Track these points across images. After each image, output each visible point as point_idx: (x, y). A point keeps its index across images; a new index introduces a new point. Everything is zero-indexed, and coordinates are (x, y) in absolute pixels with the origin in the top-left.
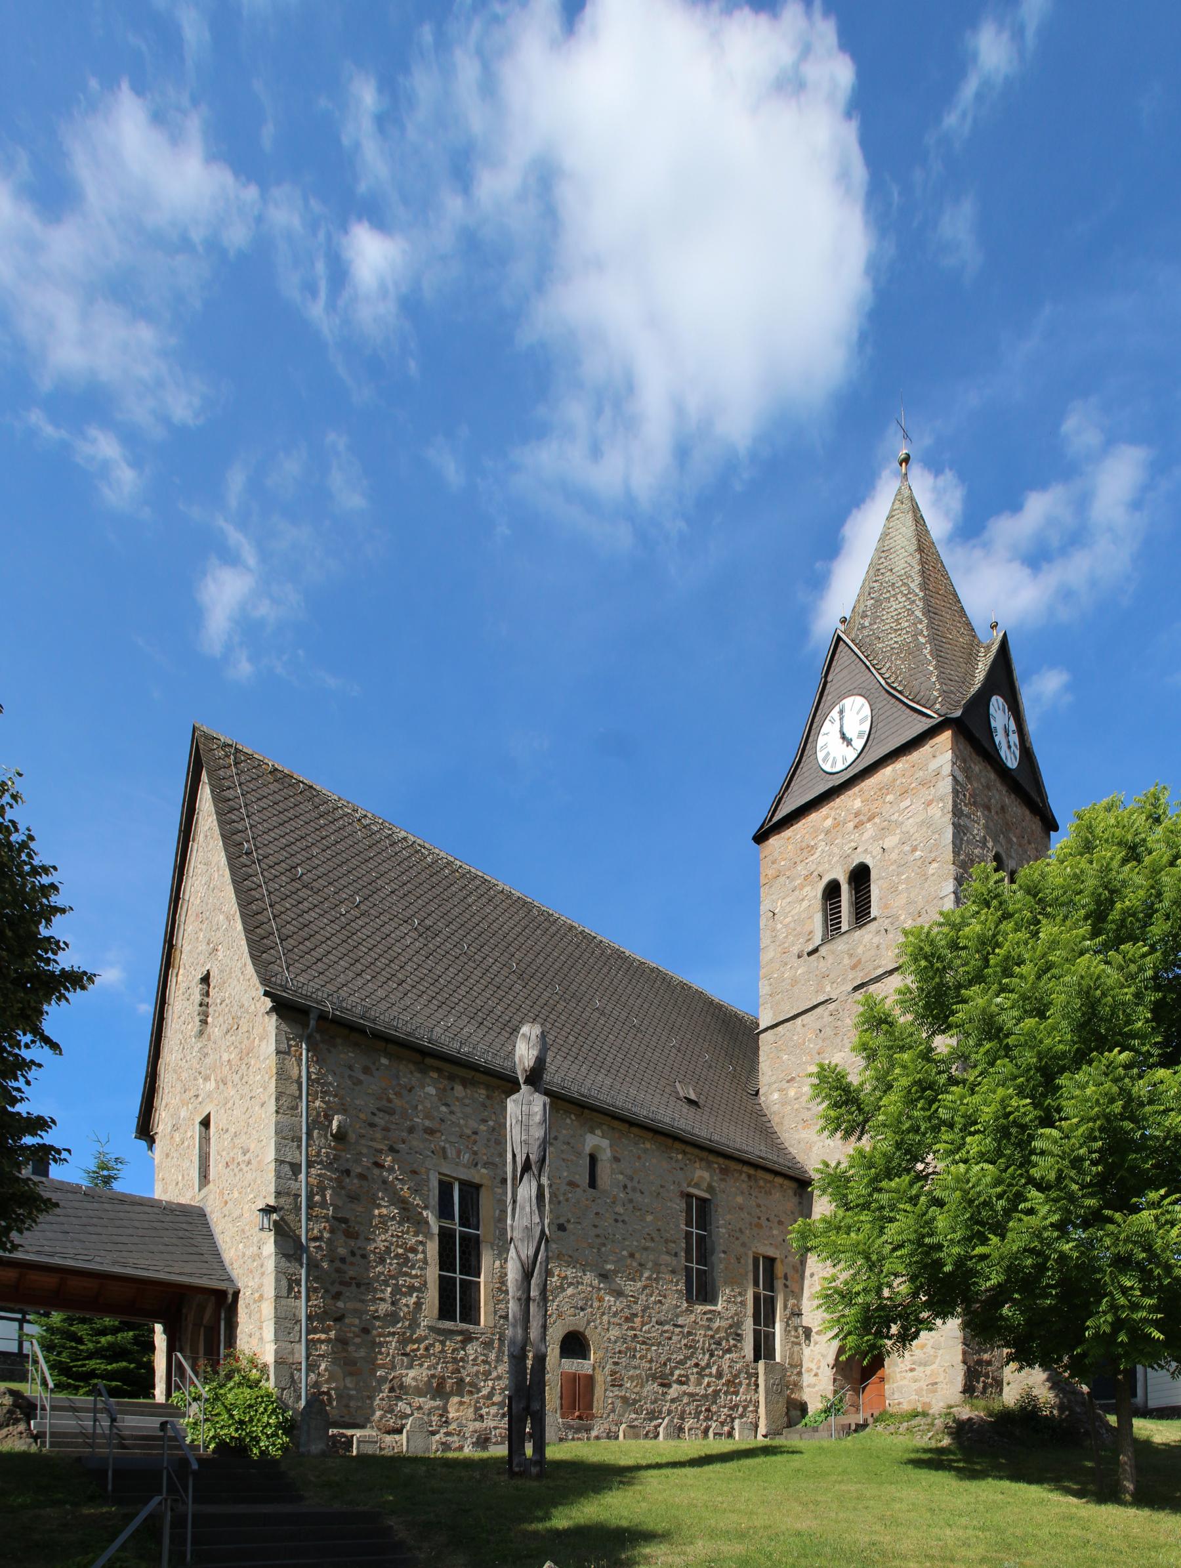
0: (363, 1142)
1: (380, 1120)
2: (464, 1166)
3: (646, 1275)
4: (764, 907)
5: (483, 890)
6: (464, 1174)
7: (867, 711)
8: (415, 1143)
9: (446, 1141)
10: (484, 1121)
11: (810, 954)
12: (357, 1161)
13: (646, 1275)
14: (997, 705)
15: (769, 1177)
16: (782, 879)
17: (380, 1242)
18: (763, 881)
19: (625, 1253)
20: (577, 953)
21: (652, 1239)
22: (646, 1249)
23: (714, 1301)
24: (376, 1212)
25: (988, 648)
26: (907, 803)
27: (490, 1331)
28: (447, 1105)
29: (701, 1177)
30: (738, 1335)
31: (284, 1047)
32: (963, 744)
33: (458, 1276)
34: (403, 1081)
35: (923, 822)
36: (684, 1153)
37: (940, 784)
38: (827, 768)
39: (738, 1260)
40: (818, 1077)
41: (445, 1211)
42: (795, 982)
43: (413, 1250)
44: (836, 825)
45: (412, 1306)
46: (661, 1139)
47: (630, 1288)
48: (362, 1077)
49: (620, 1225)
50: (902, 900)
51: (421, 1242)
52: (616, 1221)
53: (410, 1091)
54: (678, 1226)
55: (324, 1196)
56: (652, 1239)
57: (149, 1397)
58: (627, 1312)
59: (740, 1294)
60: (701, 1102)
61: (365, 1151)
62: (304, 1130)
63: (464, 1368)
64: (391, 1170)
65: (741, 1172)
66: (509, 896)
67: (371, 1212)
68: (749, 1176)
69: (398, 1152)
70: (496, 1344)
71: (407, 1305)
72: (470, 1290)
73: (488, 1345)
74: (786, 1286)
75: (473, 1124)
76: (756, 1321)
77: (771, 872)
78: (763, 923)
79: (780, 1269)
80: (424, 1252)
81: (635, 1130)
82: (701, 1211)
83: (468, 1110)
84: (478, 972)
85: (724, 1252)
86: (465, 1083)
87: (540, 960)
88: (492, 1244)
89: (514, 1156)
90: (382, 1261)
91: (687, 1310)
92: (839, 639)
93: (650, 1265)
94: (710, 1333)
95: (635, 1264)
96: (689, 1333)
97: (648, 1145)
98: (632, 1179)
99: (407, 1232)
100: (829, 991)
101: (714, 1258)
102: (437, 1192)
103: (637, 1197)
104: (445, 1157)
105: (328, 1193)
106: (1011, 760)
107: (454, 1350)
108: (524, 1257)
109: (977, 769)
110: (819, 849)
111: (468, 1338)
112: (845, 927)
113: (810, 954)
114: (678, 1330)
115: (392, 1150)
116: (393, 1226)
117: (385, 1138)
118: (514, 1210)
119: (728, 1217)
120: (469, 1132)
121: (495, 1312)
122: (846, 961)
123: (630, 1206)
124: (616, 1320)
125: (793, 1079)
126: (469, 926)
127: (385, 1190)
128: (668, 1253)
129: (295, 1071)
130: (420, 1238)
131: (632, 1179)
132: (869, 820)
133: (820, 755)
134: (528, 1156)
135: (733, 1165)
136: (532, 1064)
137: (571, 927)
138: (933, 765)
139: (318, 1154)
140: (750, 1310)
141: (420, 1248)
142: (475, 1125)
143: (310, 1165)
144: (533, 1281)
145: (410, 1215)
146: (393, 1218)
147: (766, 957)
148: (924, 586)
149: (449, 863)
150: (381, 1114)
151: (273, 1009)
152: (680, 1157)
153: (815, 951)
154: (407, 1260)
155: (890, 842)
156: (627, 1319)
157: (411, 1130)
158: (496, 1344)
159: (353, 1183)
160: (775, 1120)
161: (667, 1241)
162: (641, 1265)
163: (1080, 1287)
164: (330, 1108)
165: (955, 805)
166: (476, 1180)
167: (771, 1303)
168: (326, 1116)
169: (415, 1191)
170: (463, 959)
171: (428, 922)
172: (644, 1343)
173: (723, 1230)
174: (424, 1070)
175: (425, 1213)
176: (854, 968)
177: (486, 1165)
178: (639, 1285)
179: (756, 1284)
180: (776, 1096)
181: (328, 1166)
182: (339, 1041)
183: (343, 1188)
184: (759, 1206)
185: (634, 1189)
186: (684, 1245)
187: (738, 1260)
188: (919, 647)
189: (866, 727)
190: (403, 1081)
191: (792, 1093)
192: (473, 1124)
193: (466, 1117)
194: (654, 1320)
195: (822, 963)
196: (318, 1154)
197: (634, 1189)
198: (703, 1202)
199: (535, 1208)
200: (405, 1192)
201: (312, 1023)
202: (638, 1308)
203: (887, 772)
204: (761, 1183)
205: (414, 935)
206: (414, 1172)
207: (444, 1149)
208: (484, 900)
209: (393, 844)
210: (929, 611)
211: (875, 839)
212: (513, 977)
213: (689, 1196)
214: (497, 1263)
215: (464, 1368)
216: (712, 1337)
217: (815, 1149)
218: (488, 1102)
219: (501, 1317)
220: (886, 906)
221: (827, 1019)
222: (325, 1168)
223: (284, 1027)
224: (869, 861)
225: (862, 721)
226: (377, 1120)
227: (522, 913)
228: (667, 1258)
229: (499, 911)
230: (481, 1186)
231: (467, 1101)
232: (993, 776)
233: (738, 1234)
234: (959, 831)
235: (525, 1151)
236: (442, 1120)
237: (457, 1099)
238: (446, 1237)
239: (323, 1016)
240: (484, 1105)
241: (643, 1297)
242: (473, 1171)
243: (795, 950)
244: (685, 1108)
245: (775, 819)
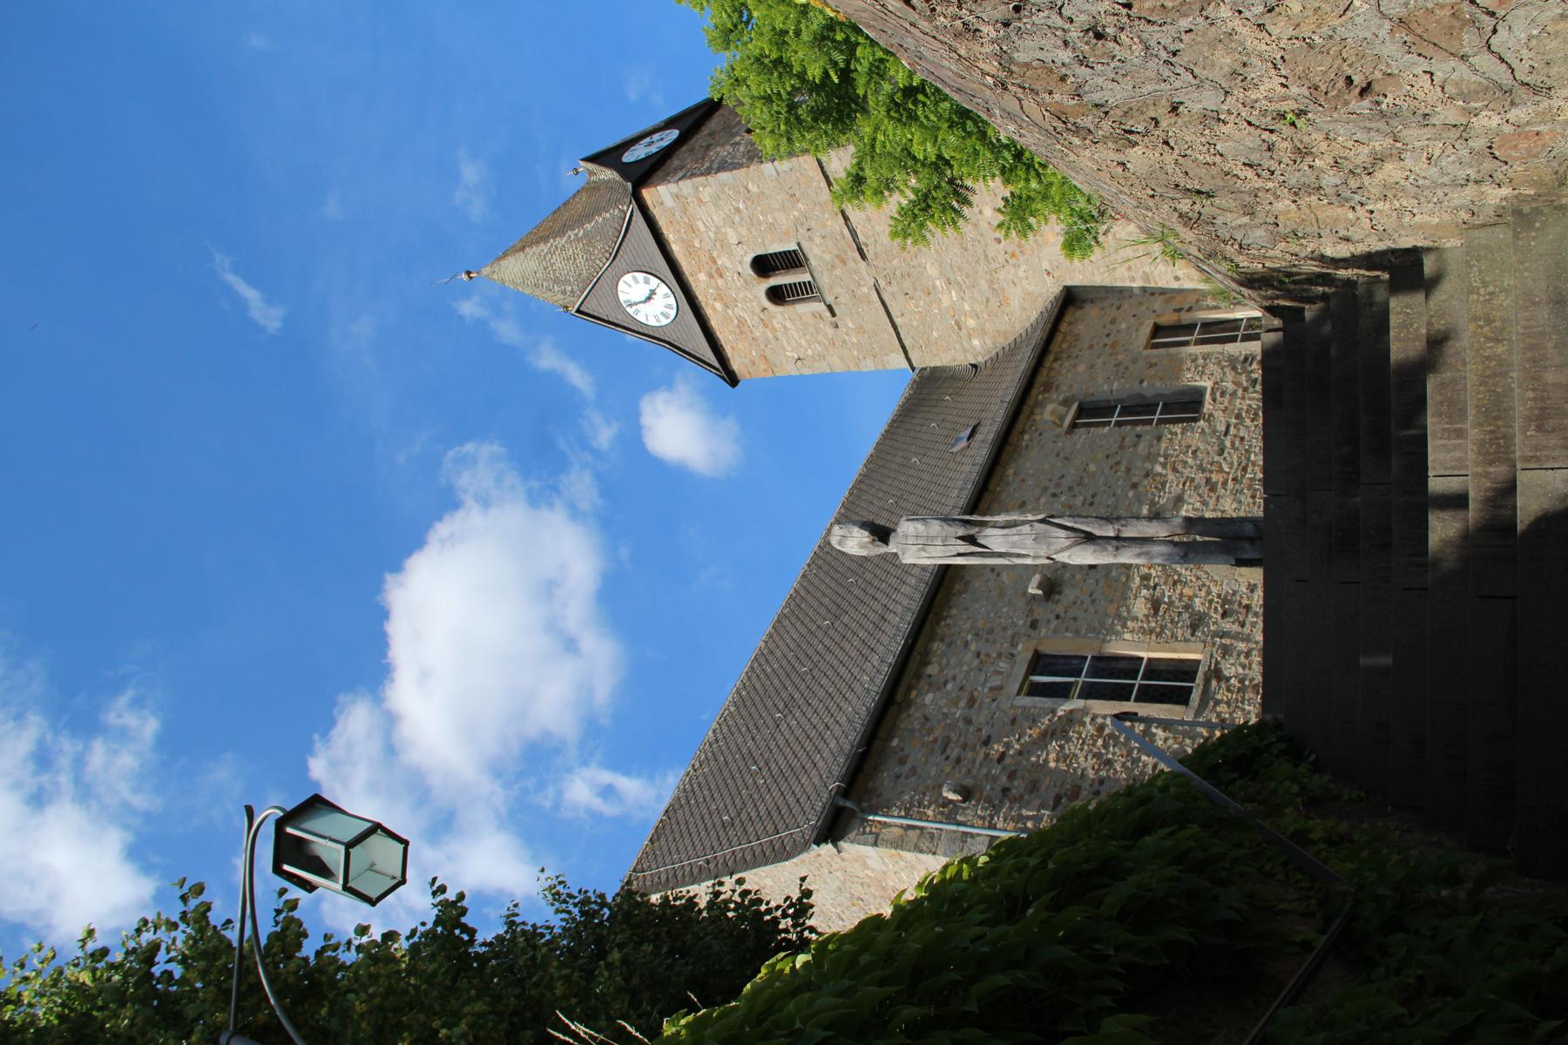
0: (975, 772)
1: (954, 752)
2: (1012, 667)
3: (1159, 469)
4: (792, 370)
5: (762, 660)
6: (1021, 669)
7: (628, 278)
8: (982, 718)
9: (983, 686)
10: (966, 644)
11: (833, 314)
12: (995, 779)
13: (1159, 469)
14: (628, 157)
15: (1059, 338)
16: (768, 353)
17: (1086, 763)
18: (770, 375)
19: (1131, 494)
20: (826, 567)
21: (1118, 463)
22: (1128, 470)
23: (1200, 392)
24: (1052, 764)
25: (591, 173)
26: (700, 223)
27: (1208, 648)
28: (945, 683)
29: (1052, 413)
30: (1246, 359)
31: (871, 838)
32: (655, 178)
33: (1138, 682)
34: (916, 725)
35: (716, 205)
36: (1022, 433)
37: (685, 192)
38: (673, 313)
39: (1151, 366)
40: (905, 238)
41: (1062, 692)
42: (860, 330)
43: (1101, 728)
44: (720, 298)
45: (1167, 734)
46: (1004, 457)
47: (1173, 488)
48: (908, 766)
49: (1097, 500)
50: (781, 217)
51: (1093, 719)
52: (1092, 504)
53: (927, 719)
54: (1105, 436)
55: (1028, 818)
56: (1118, 463)
58: (1204, 490)
59: (1194, 361)
60: (974, 422)
61: (984, 771)
62: (954, 828)
63: (1252, 680)
64: (1008, 746)
65: (1051, 369)
66: (770, 636)
67: (1051, 770)
68: (1056, 359)
69: (989, 737)
70: (1227, 641)
71: (1166, 740)
72: (1155, 669)
73: (1226, 651)
74: (1190, 309)
75: (968, 657)
76: (1233, 339)
77: (762, 366)
79: (1168, 318)
80: (1104, 717)
81: (991, 486)
82: (1091, 411)
83: (953, 661)
84: (828, 657)
85: (1142, 382)
86: (925, 663)
87: (826, 601)
88: (1104, 641)
89: (959, 555)
90: (1109, 763)
91: (1208, 421)
92: (578, 311)
93: (1148, 465)
94: (1240, 392)
95: (1145, 482)
96: (1238, 416)
97: (1011, 472)
98: (1046, 488)
99: (1080, 734)
100: (867, 289)
101: (1149, 393)
102: (1037, 699)
103: (1066, 482)
104: (1000, 688)
105: (1025, 812)
106: (673, 134)
107: (1229, 690)
108: (1068, 542)
110: (737, 304)
111: (1216, 673)
112: (806, 277)
113: (833, 314)
114: (1232, 430)
115: (987, 742)
116: (1070, 748)
117: (973, 749)
118: (1019, 556)
119: (1100, 380)
120: (976, 662)
121: (1186, 640)
122: (838, 272)
123: (1077, 489)
124: (1212, 502)
125: (957, 323)
126: (789, 668)
127: (1030, 753)
128: (1135, 445)
129: (896, 830)
130: (1088, 720)
131: (1046, 488)
132: (715, 262)
133: (664, 322)
134: (960, 538)
135: (1041, 379)
136: (866, 533)
137: (804, 576)
138: (669, 202)
139: (983, 818)
140: (1217, 348)
141: (1099, 720)
142: (970, 655)
143: (994, 828)
144: (1098, 533)
145: (1060, 730)
146: (1062, 747)
147: (839, 366)
148: (545, 239)
149: (738, 691)
150: (948, 751)
151: (835, 843)
152: (1027, 437)
153: (830, 308)
154: (1111, 736)
156: (1213, 489)
157: (968, 721)
158: (1227, 641)
159: (1018, 786)
160: (1003, 342)
161: (1122, 447)
162: (1147, 475)
164: (936, 802)
165: (702, 174)
166: (1029, 655)
167: (1208, 326)
168: (944, 806)
169: (1034, 722)
170: (815, 672)
171: (781, 706)
172: (1245, 469)
173: (1116, 385)
174: (908, 703)
175: (1060, 713)
176: (844, 262)
177: (1013, 645)
178: (1171, 477)
179: (1186, 343)
180: (976, 342)
181: (996, 809)
182: (870, 785)
183: (1022, 796)
184: (1091, 347)
185: (1058, 485)
186: (1129, 428)
187: (1151, 366)
189: (640, 276)
190: (916, 725)
191: (972, 323)
192: (968, 657)
193: (960, 664)
194: (1216, 458)
195: (842, 299)
196: (983, 818)
197: (1058, 485)
198: (1083, 411)
199: (1014, 530)
200: (1035, 732)
201: (848, 804)
202: (1200, 477)
203: (676, 249)
204: (1065, 346)
205: (789, 717)
206: (1013, 721)
207: (992, 689)
208: (770, 658)
209: (717, 741)
210: (561, 232)
211: (730, 255)
212: (837, 624)
213: (1074, 426)
214: (1127, 636)
215: (1252, 680)
216: (1245, 389)
217: (1030, 289)
218: (948, 640)
219: (1193, 635)
220: (787, 234)
221: (894, 288)
222: (998, 813)
223: (852, 835)
224: (749, 259)
225: (637, 281)
226: (954, 755)
227: (786, 623)
228: (1142, 446)
229: (781, 644)
230: (1036, 651)
231: (944, 662)
233: (1122, 369)
234: (723, 167)
235: (953, 541)
236: (961, 688)
237: (941, 671)
238: (1090, 692)
239: (845, 793)
240: (950, 645)
241: (1186, 472)
242: (1018, 659)
243: (830, 331)
244: (978, 437)
245: (717, 364)
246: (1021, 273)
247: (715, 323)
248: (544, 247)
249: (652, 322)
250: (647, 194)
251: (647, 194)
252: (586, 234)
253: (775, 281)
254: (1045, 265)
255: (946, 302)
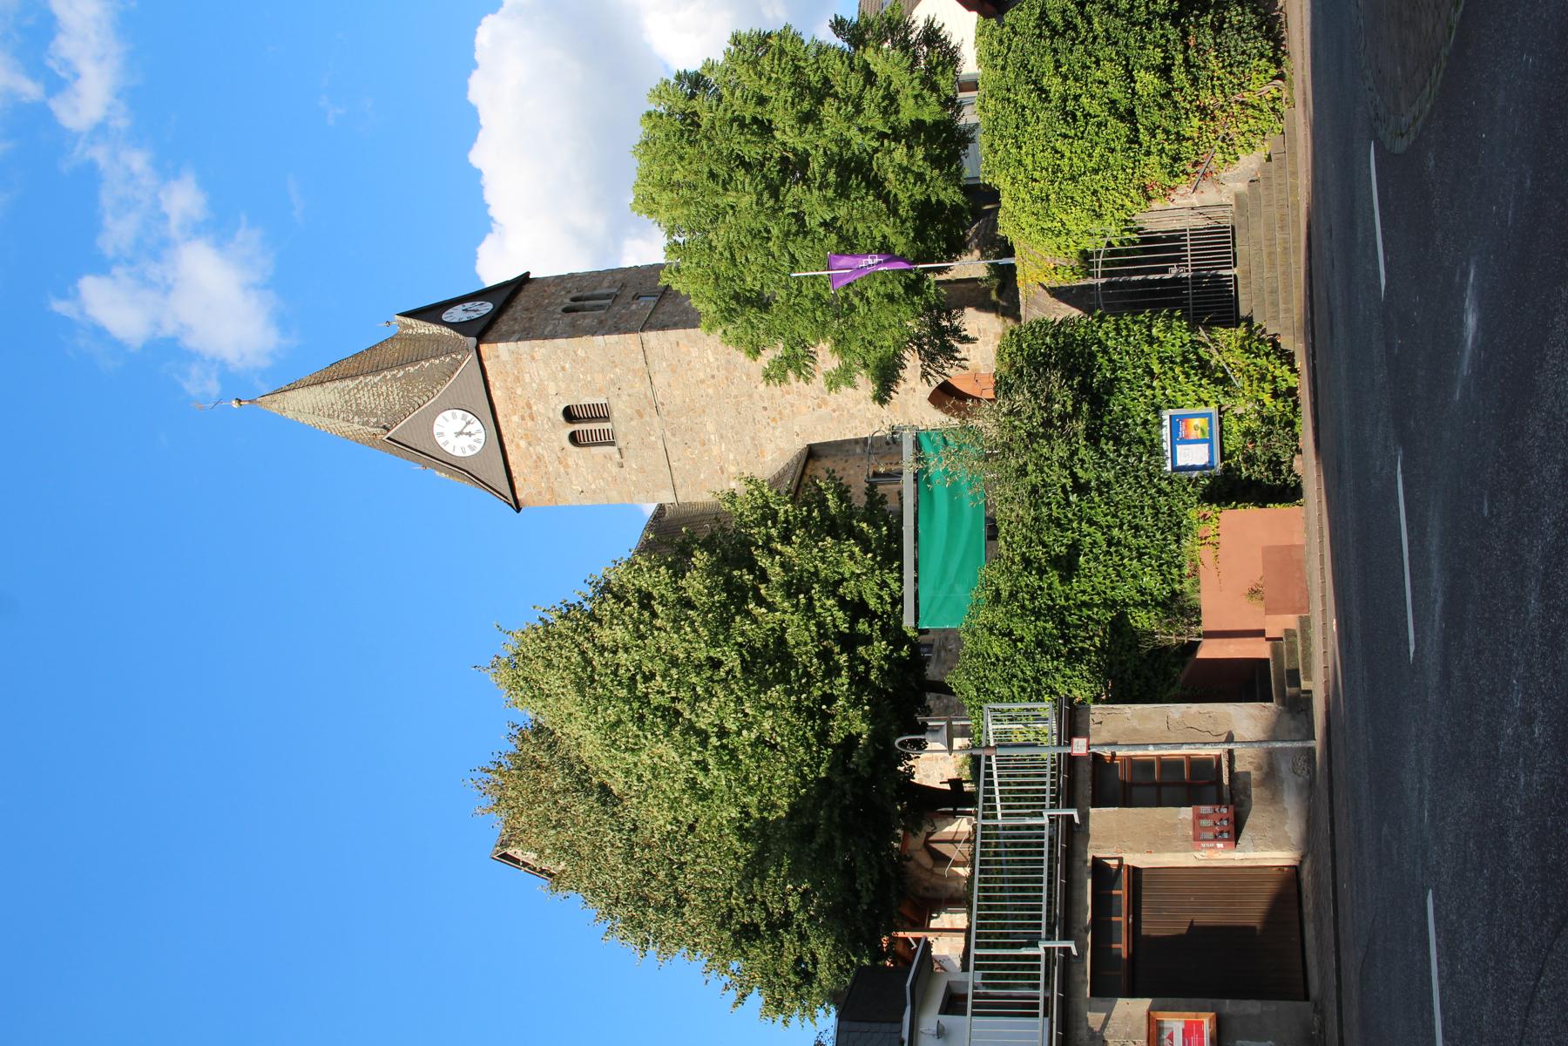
16: (556, 485)
57: (1095, 993)
78: (588, 503)
106: (486, 307)
109: (504, 328)
122: (633, 423)
132: (530, 408)
133: (469, 453)
155: (552, 390)
163: (927, 212)
176: (641, 416)
188: (406, 375)
210: (377, 370)
232: (505, 317)
246: (777, 433)
247: (511, 459)
248: (350, 384)
249: (458, 453)
250: (484, 348)
251: (484, 348)
252: (406, 375)
253: (577, 427)
254: (797, 429)
255: (715, 452)
